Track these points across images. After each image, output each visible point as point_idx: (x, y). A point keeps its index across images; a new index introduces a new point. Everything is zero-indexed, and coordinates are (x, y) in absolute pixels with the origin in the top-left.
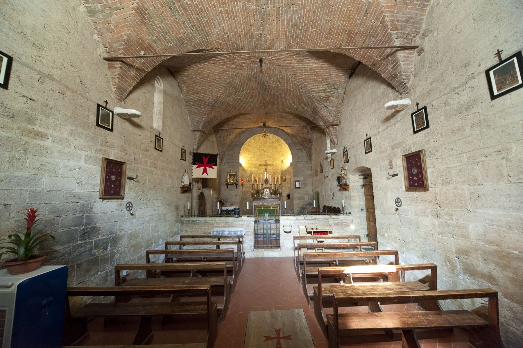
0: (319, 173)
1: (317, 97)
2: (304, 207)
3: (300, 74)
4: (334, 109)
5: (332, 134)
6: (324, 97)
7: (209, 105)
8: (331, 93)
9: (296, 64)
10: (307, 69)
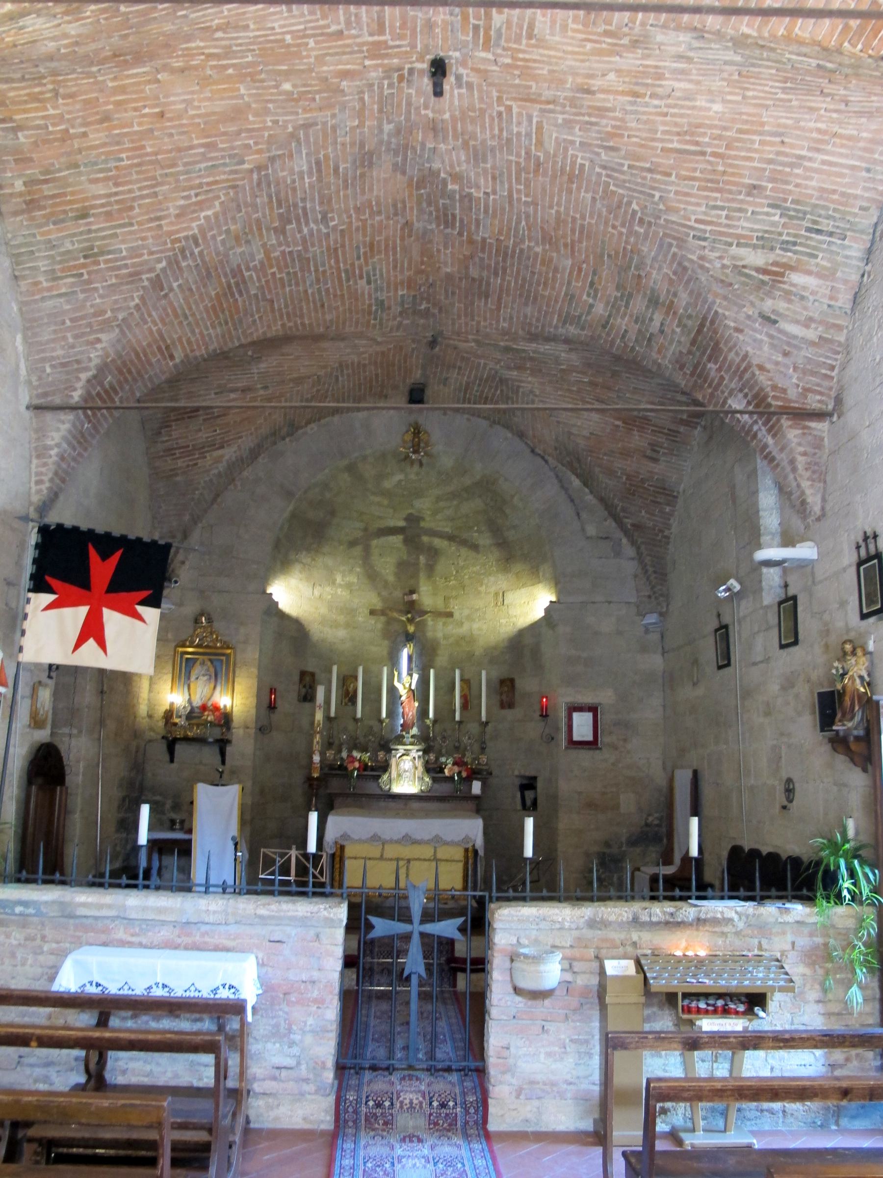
0: (710, 668)
1: (724, 266)
2: (615, 850)
3: (642, 146)
4: (811, 334)
5: (792, 462)
6: (758, 270)
7: (135, 276)
8: (795, 252)
9: (623, 93)
10: (676, 124)
